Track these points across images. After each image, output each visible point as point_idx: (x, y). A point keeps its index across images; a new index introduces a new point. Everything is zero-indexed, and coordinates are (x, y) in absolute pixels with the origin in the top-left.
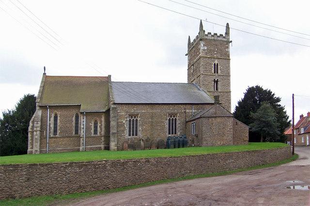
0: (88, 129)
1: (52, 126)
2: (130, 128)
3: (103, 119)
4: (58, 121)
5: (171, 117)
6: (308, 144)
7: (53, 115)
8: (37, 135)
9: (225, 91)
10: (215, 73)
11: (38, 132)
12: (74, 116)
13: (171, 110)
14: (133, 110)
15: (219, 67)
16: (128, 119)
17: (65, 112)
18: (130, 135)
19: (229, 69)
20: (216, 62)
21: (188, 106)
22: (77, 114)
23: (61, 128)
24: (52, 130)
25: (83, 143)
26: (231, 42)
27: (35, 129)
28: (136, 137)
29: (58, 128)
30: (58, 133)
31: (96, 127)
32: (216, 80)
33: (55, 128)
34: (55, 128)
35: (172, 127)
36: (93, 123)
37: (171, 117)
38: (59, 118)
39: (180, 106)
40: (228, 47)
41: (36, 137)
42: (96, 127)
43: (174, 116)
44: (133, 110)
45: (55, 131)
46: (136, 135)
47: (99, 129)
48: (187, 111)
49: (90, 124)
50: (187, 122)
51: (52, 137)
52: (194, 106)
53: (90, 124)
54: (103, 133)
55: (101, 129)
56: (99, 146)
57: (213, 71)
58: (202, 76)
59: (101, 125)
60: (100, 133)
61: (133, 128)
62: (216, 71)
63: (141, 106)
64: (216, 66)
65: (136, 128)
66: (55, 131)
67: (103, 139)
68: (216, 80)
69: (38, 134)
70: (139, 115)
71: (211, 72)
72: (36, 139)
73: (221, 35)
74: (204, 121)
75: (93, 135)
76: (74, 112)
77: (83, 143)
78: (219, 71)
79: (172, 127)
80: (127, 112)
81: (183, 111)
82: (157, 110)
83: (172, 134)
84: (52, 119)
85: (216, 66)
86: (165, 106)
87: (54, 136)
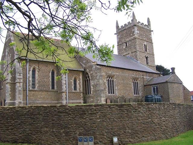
0: (69, 84)
1: (31, 79)
2: (109, 87)
3: (81, 77)
4: (37, 75)
5: (135, 80)
6: (192, 100)
7: (32, 69)
8: (20, 87)
9: (152, 65)
10: (145, 51)
11: (22, 84)
12: (51, 73)
13: (134, 75)
14: (111, 72)
15: (147, 47)
16: (108, 79)
17: (43, 67)
18: (109, 93)
19: (153, 50)
20: (145, 43)
21: (145, 74)
22: (53, 70)
23: (39, 81)
24: (31, 84)
25: (66, 98)
26: (152, 31)
27: (17, 80)
28: (114, 94)
29: (37, 82)
30: (36, 87)
31: (75, 84)
32: (147, 56)
33: (34, 81)
34: (34, 81)
35: (136, 88)
36: (73, 79)
37: (135, 80)
38: (37, 72)
39: (140, 72)
40: (150, 34)
41: (20, 88)
42: (75, 84)
43: (112, 78)
44: (111, 72)
45: (34, 85)
46: (114, 93)
47: (78, 86)
48: (144, 77)
49: (71, 81)
50: (145, 86)
51: (32, 90)
52: (148, 74)
53: (71, 81)
54: (81, 89)
55: (80, 86)
56: (79, 101)
57: (144, 50)
58: (138, 52)
59: (80, 82)
60: (79, 89)
61: (111, 87)
62: (146, 50)
63: (115, 69)
64: (145, 46)
65: (113, 87)
66: (34, 85)
67: (82, 94)
68: (147, 56)
69: (21, 85)
70: (115, 77)
71: (143, 50)
72: (20, 90)
73: (146, 25)
74: (169, 85)
75: (73, 91)
76: (51, 68)
77: (66, 98)
78: (148, 50)
79: (136, 88)
80: (106, 73)
81: (141, 77)
82: (126, 74)
83: (136, 94)
84: (31, 72)
85: (145, 46)
86: (131, 72)
87: (33, 89)
